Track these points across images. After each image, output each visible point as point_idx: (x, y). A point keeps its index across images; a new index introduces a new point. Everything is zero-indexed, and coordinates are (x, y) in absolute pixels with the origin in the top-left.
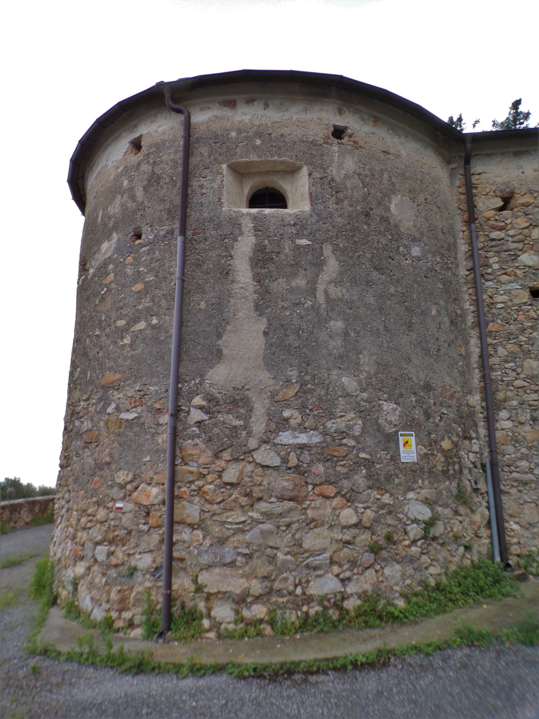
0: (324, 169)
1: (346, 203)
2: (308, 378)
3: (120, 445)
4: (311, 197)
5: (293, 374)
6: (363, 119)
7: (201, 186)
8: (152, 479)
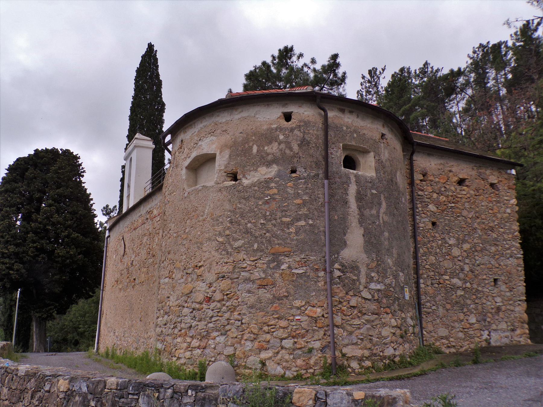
5: (374, 256)
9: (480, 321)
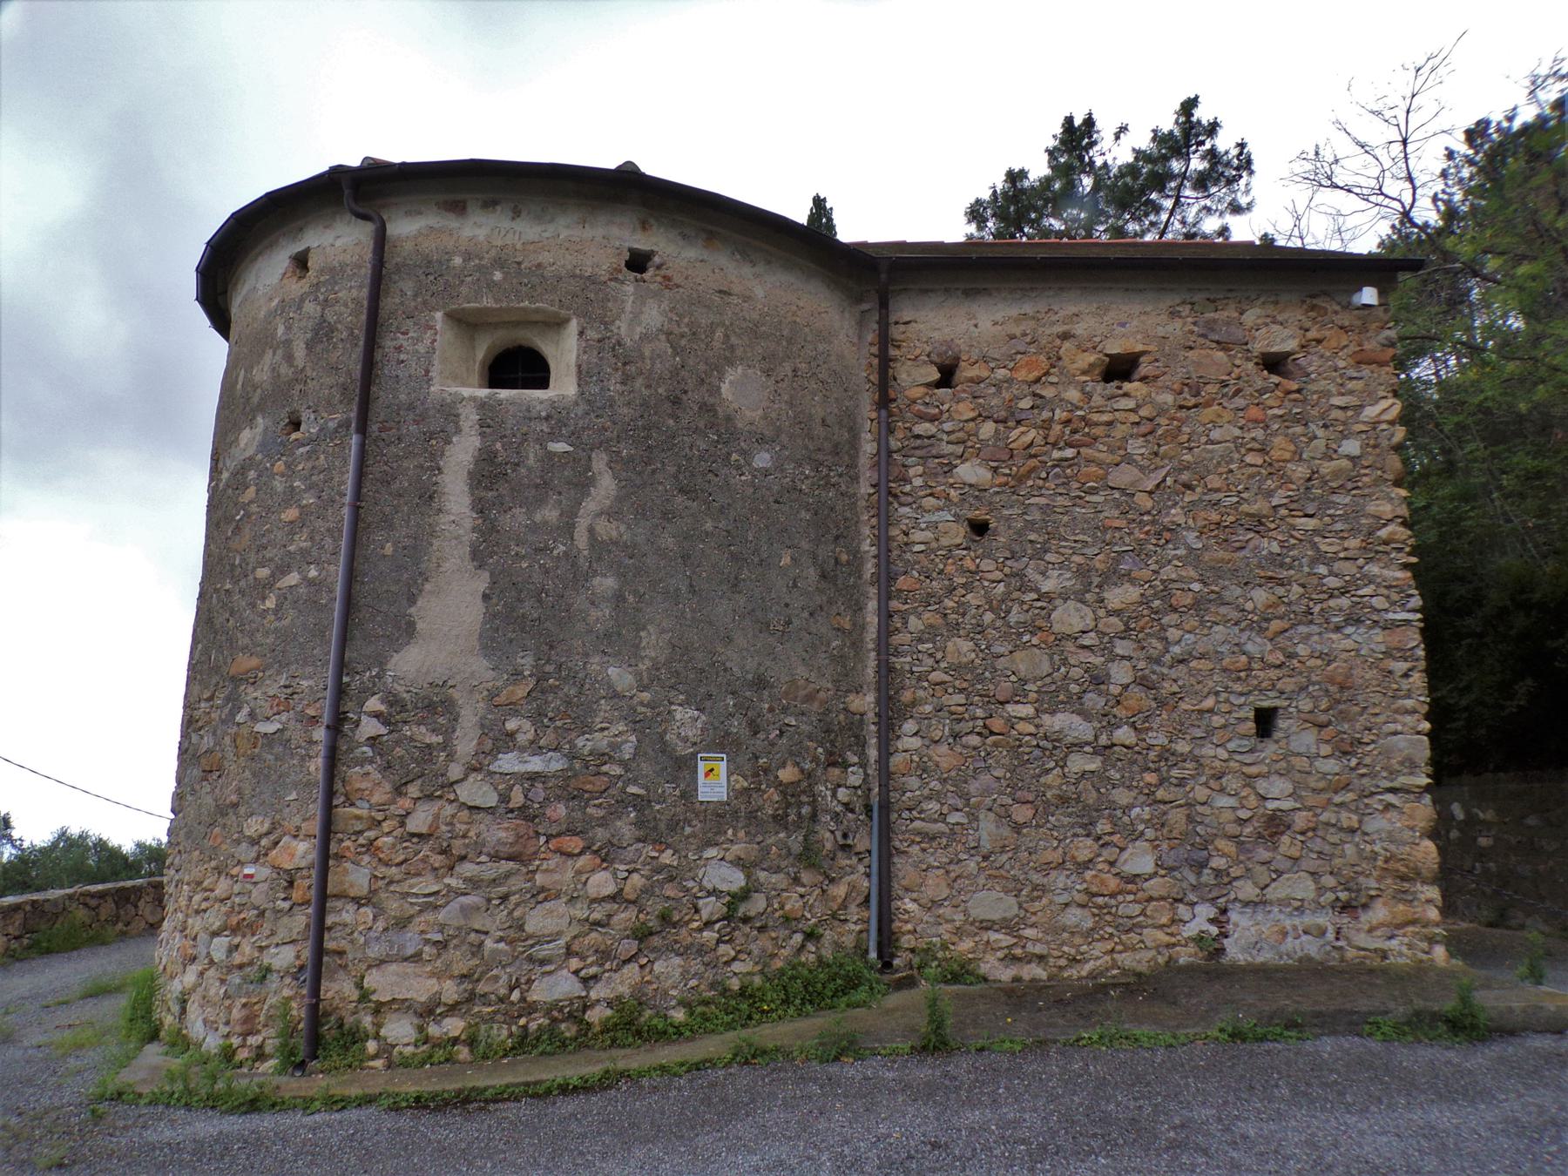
0: (606, 324)
1: (639, 382)
2: (549, 668)
3: (254, 775)
4: (579, 372)
5: (526, 662)
6: (684, 237)
7: (399, 349)
8: (298, 829)
9: (1172, 869)
